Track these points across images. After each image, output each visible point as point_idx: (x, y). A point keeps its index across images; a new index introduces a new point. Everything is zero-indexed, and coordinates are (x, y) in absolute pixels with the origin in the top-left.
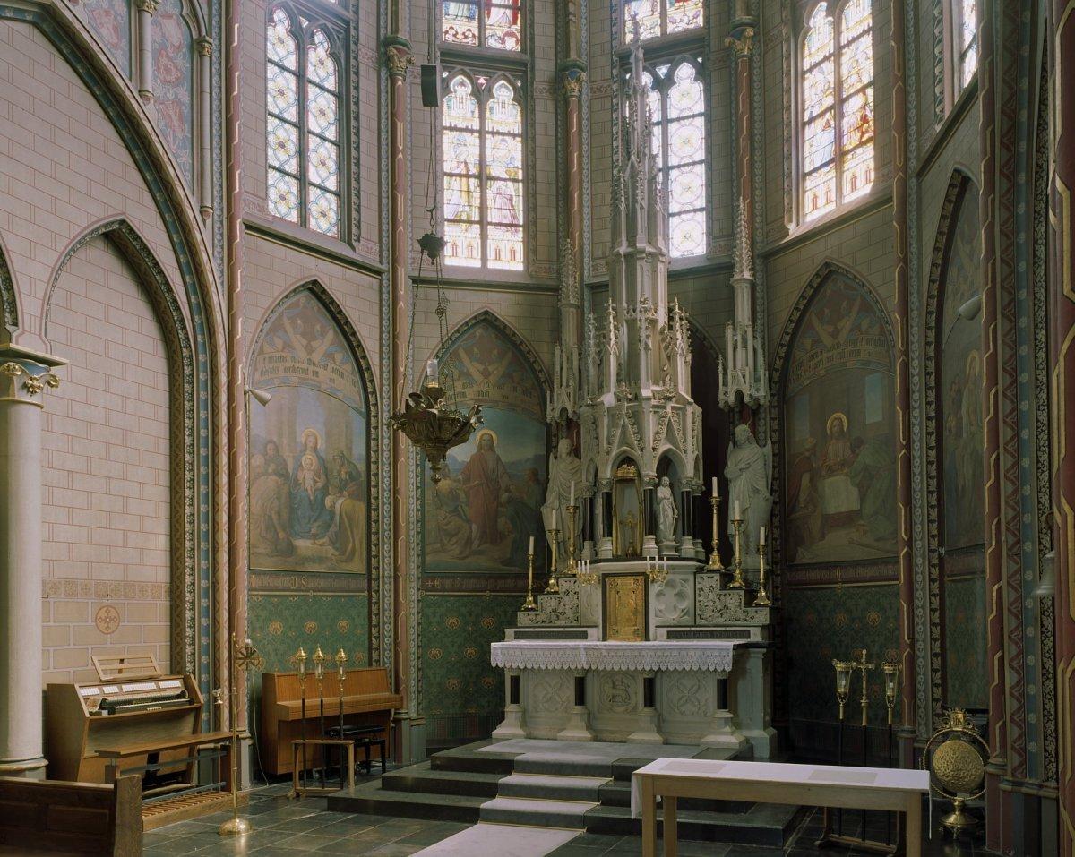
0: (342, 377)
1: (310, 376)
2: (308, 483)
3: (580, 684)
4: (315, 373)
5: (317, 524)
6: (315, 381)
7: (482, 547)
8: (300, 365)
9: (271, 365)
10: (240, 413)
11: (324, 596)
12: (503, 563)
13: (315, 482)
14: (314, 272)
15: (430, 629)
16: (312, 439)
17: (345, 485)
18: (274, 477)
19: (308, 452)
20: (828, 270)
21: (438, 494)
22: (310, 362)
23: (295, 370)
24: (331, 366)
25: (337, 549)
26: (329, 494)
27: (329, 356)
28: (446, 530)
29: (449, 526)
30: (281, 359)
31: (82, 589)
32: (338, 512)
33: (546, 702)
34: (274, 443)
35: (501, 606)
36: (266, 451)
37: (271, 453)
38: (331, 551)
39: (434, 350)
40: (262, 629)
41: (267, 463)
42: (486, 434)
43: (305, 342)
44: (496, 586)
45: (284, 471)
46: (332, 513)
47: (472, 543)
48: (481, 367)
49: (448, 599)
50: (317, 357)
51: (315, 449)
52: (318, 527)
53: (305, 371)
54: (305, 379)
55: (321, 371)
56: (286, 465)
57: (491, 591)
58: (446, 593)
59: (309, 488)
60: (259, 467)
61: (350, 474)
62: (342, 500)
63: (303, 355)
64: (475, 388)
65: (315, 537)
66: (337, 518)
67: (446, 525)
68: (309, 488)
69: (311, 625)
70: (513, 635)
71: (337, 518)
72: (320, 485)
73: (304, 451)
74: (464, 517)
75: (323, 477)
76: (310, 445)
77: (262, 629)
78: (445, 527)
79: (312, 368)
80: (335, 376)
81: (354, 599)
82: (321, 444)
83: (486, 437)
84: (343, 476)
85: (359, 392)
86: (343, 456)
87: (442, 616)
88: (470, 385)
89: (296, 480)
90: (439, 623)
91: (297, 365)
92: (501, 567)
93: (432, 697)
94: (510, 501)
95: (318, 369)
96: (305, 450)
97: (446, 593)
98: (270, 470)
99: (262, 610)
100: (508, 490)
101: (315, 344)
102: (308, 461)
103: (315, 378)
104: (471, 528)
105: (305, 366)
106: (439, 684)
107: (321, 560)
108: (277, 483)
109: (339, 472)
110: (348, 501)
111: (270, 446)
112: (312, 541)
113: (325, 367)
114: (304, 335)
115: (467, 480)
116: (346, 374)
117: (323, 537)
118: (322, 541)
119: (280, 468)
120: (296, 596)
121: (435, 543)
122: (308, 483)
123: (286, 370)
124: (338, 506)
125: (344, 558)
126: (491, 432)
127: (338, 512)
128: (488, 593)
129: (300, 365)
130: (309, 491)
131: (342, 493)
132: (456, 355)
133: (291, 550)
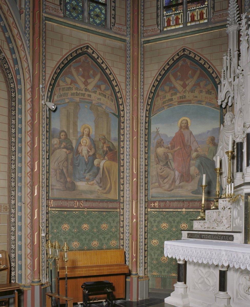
0: (105, 97)
1: (86, 97)
2: (85, 153)
3: (223, 276)
4: (89, 96)
5: (88, 174)
6: (89, 100)
7: (181, 184)
8: (81, 92)
9: (64, 92)
10: (37, 114)
11: (93, 211)
12: (193, 192)
13: (88, 152)
14: (87, 42)
15: (172, 229)
16: (87, 130)
17: (106, 153)
18: (65, 150)
19: (84, 136)
20: (86, 50)
21: (157, 156)
22: (86, 90)
23: (77, 94)
24: (98, 92)
25: (101, 187)
26: (97, 158)
27: (98, 86)
28: (161, 176)
29: (163, 173)
30: (69, 89)
31: (4, 208)
32: (101, 168)
33: (201, 283)
34: (65, 132)
35: (93, 218)
36: (60, 136)
37: (63, 137)
38: (97, 187)
39: (155, 77)
40: (57, 228)
41: (60, 143)
42: (184, 120)
43: (83, 80)
44: (189, 206)
45: (70, 147)
46: (98, 169)
47: (175, 182)
48: (181, 83)
49: (162, 213)
50: (90, 87)
51: (89, 135)
52: (90, 175)
53: (83, 95)
54: (82, 99)
55: (93, 95)
56: (72, 143)
57: (185, 209)
58: (161, 210)
59: (85, 155)
60: (56, 144)
61: (109, 147)
62: (104, 161)
63: (82, 86)
64: (178, 95)
65: (88, 180)
66: (101, 170)
67: (161, 173)
68: (85, 155)
69: (85, 226)
70: (187, 235)
71: (101, 170)
72: (91, 153)
73: (82, 136)
74: (171, 168)
75: (93, 149)
76: (86, 133)
77: (57, 228)
78: (161, 174)
79: (87, 93)
80: (100, 97)
81: (111, 213)
82: (93, 133)
83: (184, 122)
84: (105, 149)
85: (115, 105)
86: (105, 138)
87: (158, 222)
88: (175, 94)
89: (77, 152)
90: (157, 226)
91: (78, 92)
92: (191, 195)
93: (153, 266)
94: (198, 157)
95: (90, 93)
96: (83, 135)
97: (161, 210)
98: (62, 146)
99: (58, 218)
100: (196, 151)
101: (89, 81)
102: (84, 141)
103: (89, 98)
104: (175, 173)
105: (83, 92)
106: (157, 259)
107: (92, 192)
108: (66, 152)
109: (103, 147)
110: (108, 162)
111: (62, 134)
112: (86, 183)
113: (95, 92)
114: (83, 76)
115: (173, 147)
116: (107, 96)
117: (93, 180)
118: (92, 182)
119: (68, 145)
120: (77, 211)
121: (155, 183)
122: (85, 153)
123: (73, 94)
124: (102, 165)
125: (105, 191)
126: (184, 118)
127: (101, 168)
128: (184, 210)
129: (81, 92)
130: (85, 157)
131: (104, 157)
132: (168, 79)
133: (73, 187)
